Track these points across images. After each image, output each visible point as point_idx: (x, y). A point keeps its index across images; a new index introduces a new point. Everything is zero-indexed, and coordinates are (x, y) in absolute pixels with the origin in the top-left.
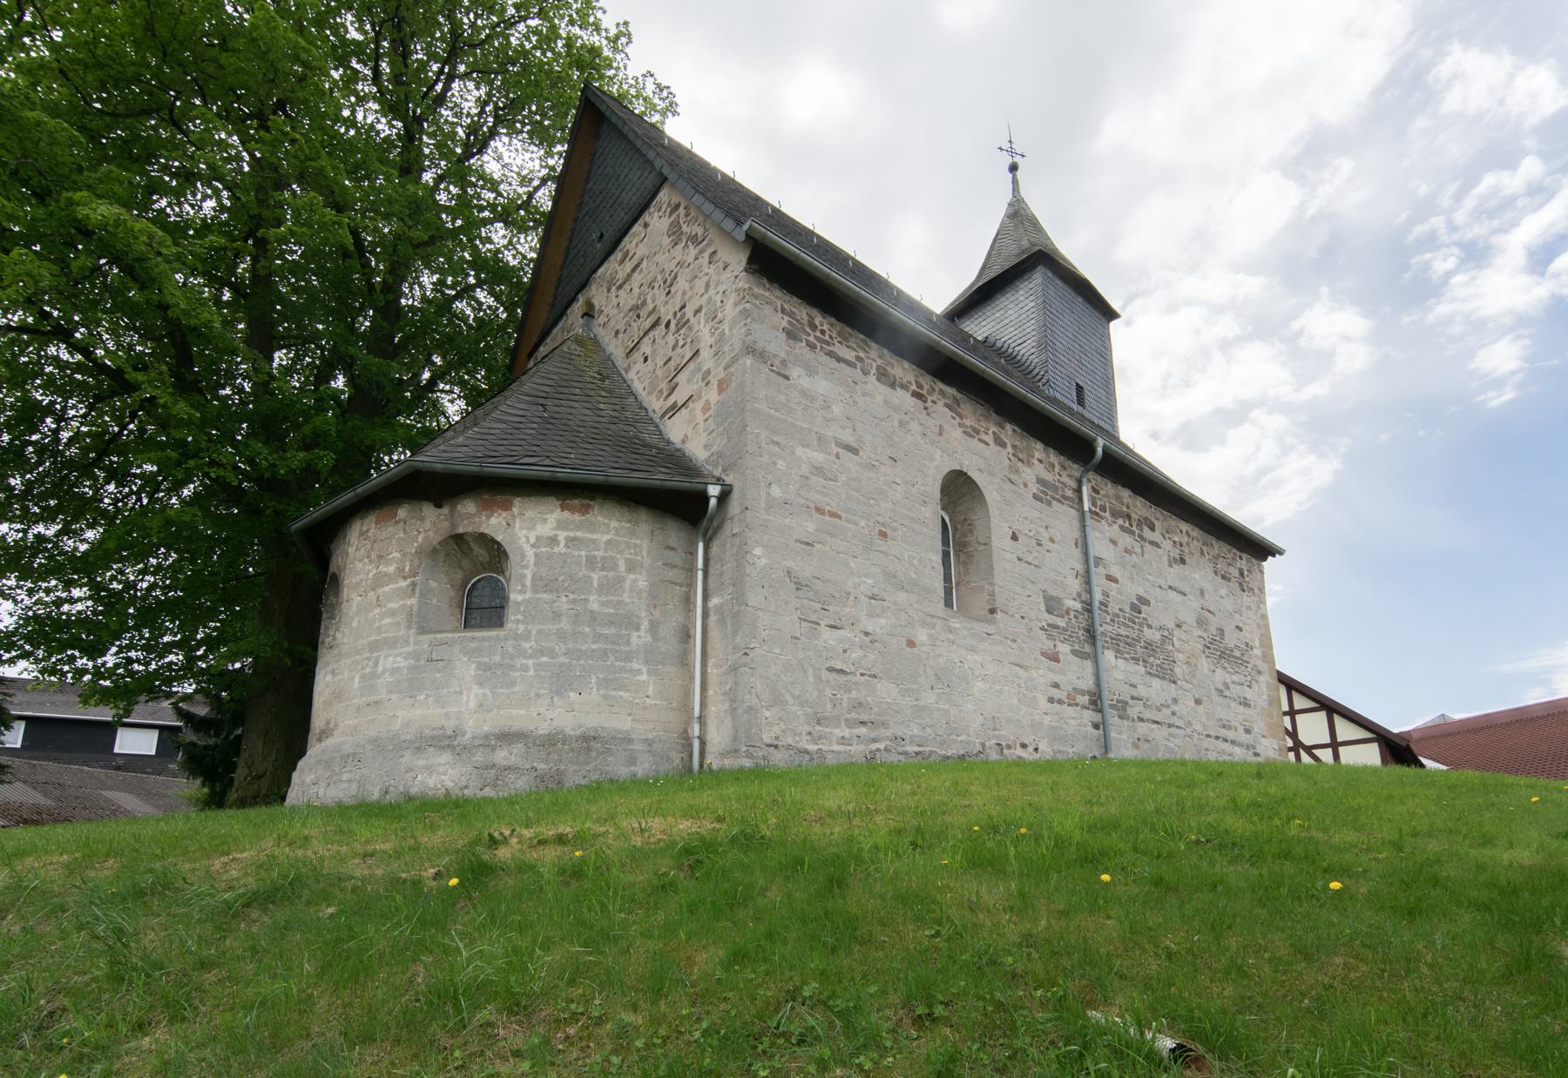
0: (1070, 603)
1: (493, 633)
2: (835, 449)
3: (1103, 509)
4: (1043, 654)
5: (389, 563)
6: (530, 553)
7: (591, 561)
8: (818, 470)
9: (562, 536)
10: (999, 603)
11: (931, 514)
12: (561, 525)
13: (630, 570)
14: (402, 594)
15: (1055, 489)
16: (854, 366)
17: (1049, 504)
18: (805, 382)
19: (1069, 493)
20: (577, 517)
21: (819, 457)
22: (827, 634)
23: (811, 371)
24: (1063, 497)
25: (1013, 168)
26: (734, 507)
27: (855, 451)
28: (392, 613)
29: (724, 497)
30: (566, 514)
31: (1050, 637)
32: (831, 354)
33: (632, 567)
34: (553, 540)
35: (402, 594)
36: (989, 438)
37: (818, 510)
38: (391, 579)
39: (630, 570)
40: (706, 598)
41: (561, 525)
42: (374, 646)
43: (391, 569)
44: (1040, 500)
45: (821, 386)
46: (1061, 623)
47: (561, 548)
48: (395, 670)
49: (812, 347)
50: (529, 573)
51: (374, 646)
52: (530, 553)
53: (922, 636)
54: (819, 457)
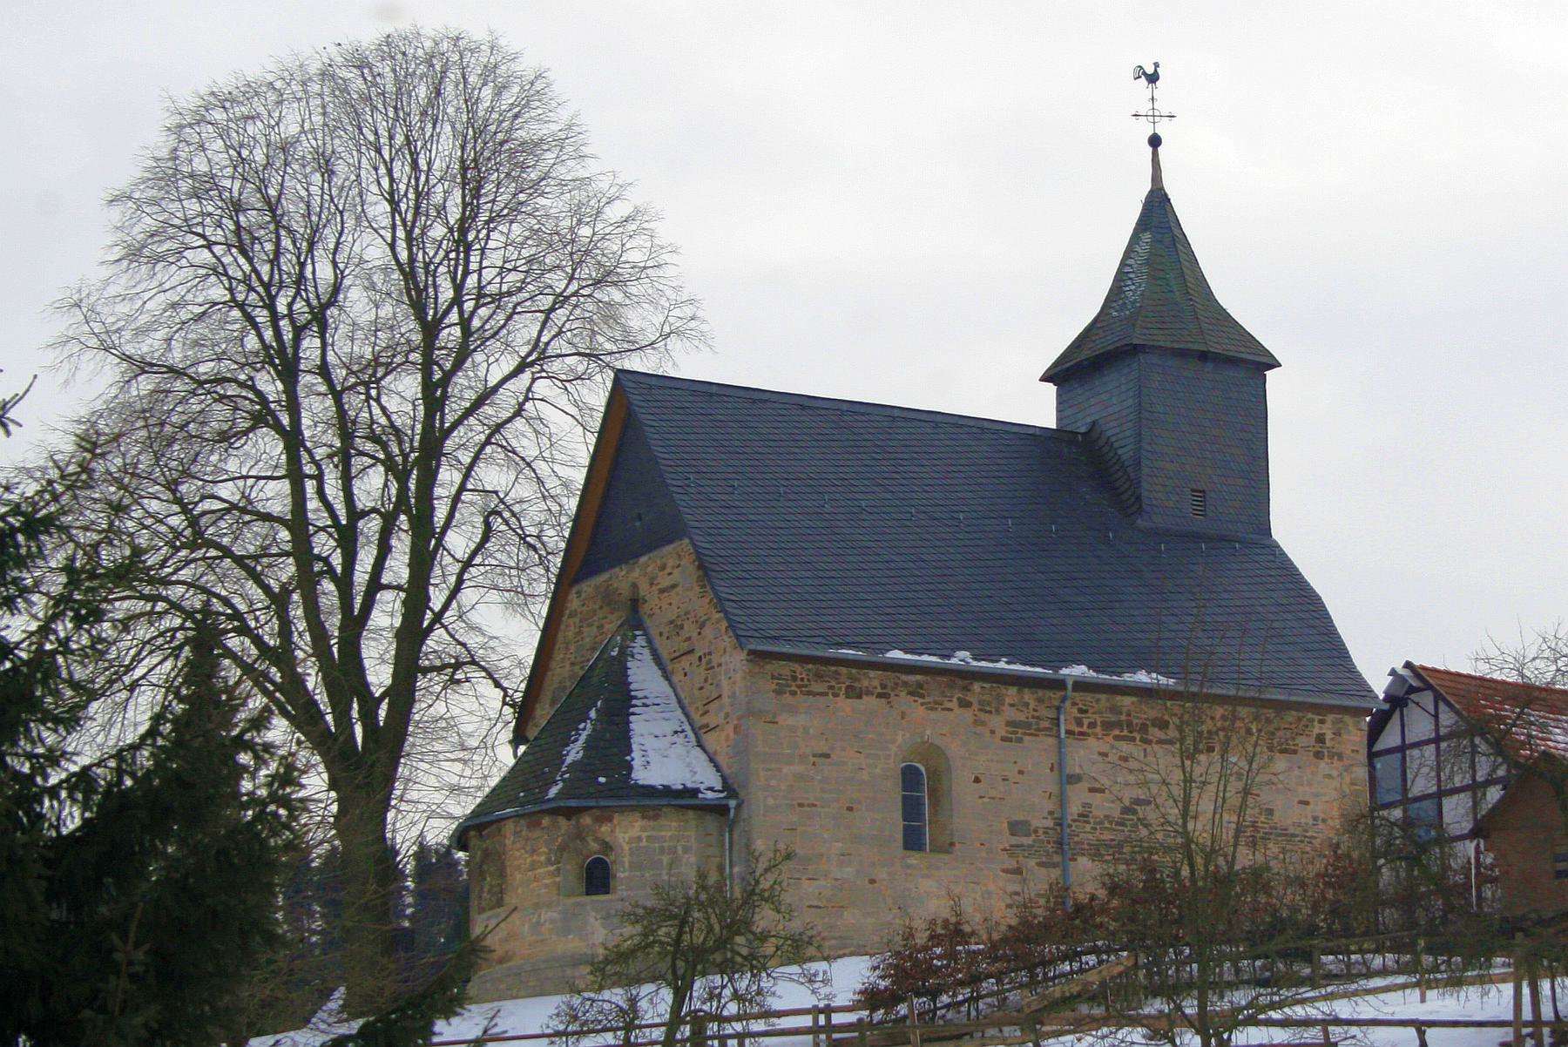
0: (1037, 823)
1: (602, 897)
2: (812, 759)
3: (1092, 725)
4: (1004, 871)
5: (539, 854)
6: (626, 847)
7: (662, 850)
8: (800, 777)
9: (644, 835)
10: (956, 840)
11: (896, 795)
12: (643, 829)
13: (685, 852)
14: (552, 874)
15: (1029, 726)
16: (826, 694)
17: (1020, 740)
18: (791, 721)
19: (1047, 724)
20: (652, 823)
21: (799, 769)
22: (806, 884)
23: (794, 711)
24: (1038, 730)
25: (1155, 141)
26: (744, 814)
27: (827, 756)
28: (546, 886)
29: (738, 807)
30: (645, 822)
31: (1012, 855)
32: (809, 693)
33: (686, 850)
34: (639, 838)
35: (552, 874)
36: (954, 704)
37: (801, 805)
38: (542, 865)
39: (685, 852)
40: (731, 866)
41: (643, 829)
42: (537, 906)
43: (543, 858)
44: (1010, 740)
45: (800, 720)
46: (1027, 841)
47: (644, 843)
48: (553, 921)
49: (794, 693)
50: (626, 860)
51: (537, 906)
52: (626, 847)
53: (882, 874)
54: (799, 769)
